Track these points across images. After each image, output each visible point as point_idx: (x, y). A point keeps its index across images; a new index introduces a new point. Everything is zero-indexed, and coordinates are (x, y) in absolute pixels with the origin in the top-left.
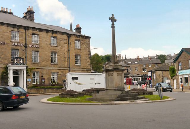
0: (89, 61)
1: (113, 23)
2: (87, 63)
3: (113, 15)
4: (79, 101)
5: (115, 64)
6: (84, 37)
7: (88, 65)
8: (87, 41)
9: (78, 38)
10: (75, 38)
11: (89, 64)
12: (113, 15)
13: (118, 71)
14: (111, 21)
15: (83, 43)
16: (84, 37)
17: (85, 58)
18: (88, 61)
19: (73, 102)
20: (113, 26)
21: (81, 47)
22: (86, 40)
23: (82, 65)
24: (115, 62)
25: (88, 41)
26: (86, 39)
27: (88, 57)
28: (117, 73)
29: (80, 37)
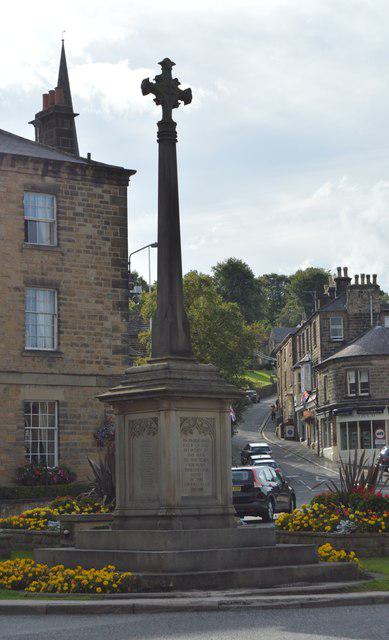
0: (116, 329)
1: (167, 114)
2: (107, 341)
3: (167, 65)
4: (107, 590)
5: (173, 365)
6: (84, 175)
7: (108, 353)
8: (107, 197)
9: (49, 180)
10: (23, 179)
11: (119, 343)
12: (167, 65)
13: (185, 404)
14: (157, 101)
15: (79, 209)
16: (84, 175)
17: (92, 306)
18: (108, 324)
19: (337, 581)
20: (167, 134)
21: (65, 235)
22: (98, 191)
23: (71, 353)
24: (173, 352)
25: (114, 200)
26: (97, 182)
27: (109, 303)
28: (184, 420)
29: (56, 174)
